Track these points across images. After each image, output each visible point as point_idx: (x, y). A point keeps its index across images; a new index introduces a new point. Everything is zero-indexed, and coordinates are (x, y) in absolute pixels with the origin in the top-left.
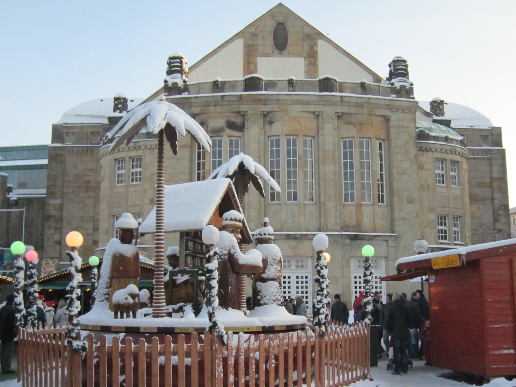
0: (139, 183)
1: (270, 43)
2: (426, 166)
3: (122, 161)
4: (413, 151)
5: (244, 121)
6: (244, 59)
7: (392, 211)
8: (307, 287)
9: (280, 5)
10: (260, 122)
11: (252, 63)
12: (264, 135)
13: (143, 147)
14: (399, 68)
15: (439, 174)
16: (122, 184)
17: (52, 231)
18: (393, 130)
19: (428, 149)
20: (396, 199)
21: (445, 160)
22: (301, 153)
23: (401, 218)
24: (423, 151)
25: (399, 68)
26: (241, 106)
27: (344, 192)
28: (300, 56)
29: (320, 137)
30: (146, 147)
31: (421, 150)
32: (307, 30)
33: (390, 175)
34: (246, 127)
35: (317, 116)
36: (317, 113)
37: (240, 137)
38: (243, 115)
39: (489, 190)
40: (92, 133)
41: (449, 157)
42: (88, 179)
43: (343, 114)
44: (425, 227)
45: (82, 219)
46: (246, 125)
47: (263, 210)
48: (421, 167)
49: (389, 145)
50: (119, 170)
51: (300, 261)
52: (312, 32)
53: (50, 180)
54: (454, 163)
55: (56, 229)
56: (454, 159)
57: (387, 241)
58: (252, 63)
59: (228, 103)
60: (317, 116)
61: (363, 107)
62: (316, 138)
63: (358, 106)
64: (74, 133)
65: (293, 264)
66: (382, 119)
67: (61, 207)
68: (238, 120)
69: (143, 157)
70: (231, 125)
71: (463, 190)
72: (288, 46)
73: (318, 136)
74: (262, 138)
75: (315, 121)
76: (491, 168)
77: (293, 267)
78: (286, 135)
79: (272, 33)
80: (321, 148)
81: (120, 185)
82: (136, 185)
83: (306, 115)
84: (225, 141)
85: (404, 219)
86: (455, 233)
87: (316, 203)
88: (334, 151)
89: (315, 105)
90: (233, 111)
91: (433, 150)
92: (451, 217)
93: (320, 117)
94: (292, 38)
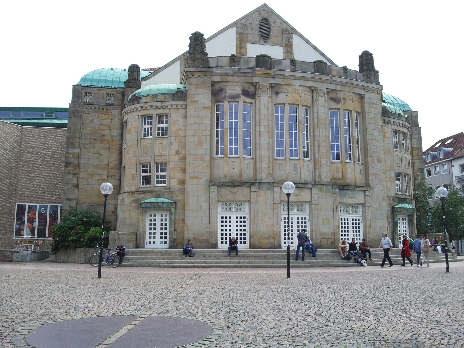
0: (164, 136)
1: (257, 33)
2: (387, 135)
3: (148, 117)
4: (381, 123)
5: (256, 90)
6: (237, 44)
8: (222, 226)
9: (265, 5)
10: (269, 93)
13: (169, 107)
14: (366, 60)
17: (71, 176)
18: (366, 105)
19: (389, 122)
20: (370, 159)
21: (399, 131)
24: (385, 123)
25: (366, 60)
26: (254, 78)
28: (280, 45)
29: (315, 108)
30: (172, 106)
32: (285, 26)
34: (257, 96)
35: (312, 90)
37: (252, 103)
38: (255, 86)
40: (107, 94)
41: (402, 129)
42: (104, 132)
43: (332, 90)
45: (97, 166)
46: (257, 93)
47: (271, 164)
48: (385, 136)
51: (239, 205)
53: (70, 132)
55: (74, 174)
57: (365, 191)
59: (243, 75)
62: (311, 108)
63: (342, 85)
64: (91, 93)
65: (234, 207)
67: (79, 156)
68: (252, 89)
69: (169, 115)
70: (246, 93)
72: (270, 37)
74: (270, 104)
75: (310, 94)
77: (234, 210)
78: (289, 104)
79: (259, 25)
80: (315, 116)
82: (163, 138)
85: (375, 175)
89: (311, 81)
90: (247, 81)
92: (403, 174)
93: (315, 91)
94: (274, 30)
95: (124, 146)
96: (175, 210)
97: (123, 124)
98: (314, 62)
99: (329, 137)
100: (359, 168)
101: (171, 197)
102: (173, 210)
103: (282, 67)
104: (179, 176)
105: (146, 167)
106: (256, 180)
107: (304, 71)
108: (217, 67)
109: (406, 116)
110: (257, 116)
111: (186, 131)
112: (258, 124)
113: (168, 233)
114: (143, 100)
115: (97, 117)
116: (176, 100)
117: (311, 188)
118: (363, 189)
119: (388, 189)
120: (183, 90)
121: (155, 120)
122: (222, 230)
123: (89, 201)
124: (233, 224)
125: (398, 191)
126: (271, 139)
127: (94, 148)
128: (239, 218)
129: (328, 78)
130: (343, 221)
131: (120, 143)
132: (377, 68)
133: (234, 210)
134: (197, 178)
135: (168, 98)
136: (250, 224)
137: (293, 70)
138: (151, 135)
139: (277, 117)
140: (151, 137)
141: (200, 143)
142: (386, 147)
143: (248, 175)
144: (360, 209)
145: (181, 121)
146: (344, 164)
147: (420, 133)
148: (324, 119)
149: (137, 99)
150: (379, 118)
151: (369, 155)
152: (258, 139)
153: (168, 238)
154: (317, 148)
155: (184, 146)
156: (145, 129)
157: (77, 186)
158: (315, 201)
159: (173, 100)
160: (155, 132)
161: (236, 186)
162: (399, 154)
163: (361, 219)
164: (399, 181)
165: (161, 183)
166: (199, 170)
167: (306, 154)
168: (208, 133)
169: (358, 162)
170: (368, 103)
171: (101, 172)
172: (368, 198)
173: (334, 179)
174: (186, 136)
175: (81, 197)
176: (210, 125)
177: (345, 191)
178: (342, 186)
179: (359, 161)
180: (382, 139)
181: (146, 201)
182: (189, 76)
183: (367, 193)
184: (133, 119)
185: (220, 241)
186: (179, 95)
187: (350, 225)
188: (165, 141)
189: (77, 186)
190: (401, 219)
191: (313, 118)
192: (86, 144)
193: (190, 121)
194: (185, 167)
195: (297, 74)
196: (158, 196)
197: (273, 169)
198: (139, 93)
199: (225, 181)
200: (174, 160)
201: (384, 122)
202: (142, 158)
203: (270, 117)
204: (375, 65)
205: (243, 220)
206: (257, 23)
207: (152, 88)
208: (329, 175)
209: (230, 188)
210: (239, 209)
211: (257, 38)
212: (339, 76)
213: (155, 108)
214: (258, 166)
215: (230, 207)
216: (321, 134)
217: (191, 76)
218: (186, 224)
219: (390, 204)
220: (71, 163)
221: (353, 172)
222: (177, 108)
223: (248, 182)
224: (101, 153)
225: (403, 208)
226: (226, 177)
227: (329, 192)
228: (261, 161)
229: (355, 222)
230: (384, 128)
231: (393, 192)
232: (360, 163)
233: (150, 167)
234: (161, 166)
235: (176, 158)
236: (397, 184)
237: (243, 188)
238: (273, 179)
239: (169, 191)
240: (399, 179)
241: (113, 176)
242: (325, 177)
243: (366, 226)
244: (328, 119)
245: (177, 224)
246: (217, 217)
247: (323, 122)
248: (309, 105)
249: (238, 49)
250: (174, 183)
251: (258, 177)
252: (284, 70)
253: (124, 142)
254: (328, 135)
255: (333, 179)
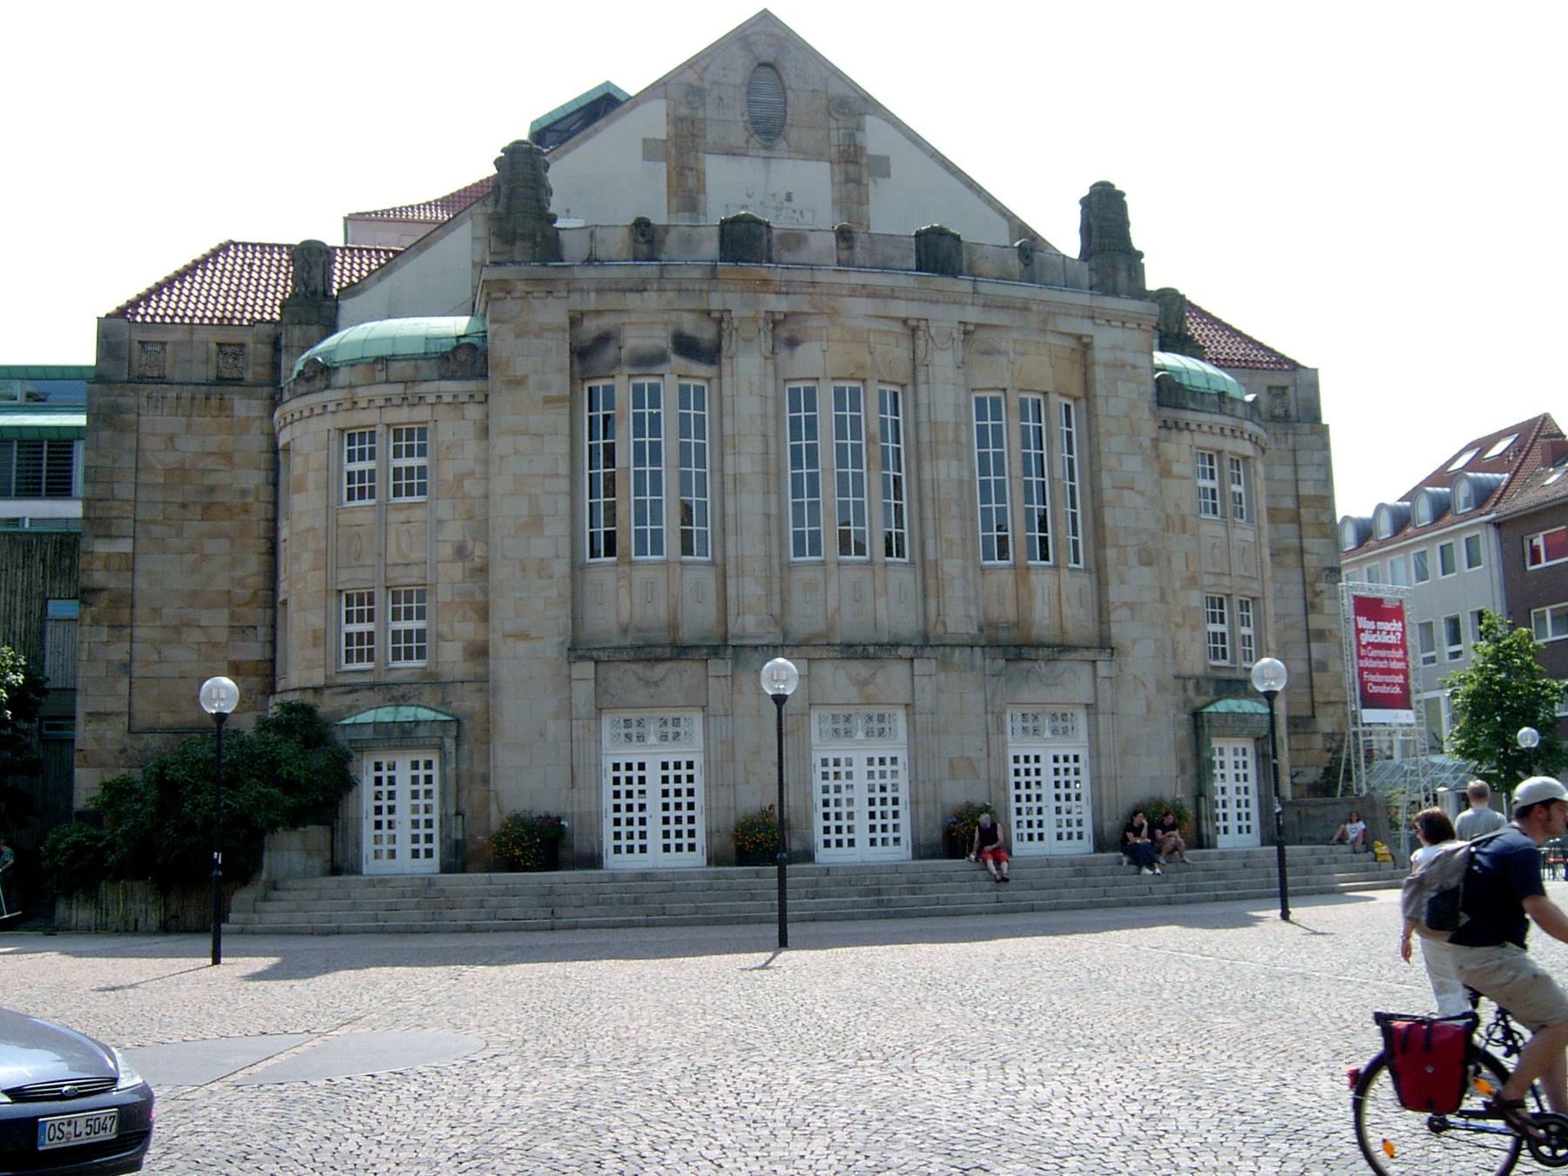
0: (416, 499)
2: (1177, 469)
4: (1148, 428)
5: (720, 337)
7: (1101, 584)
8: (617, 795)
9: (765, 16)
10: (765, 342)
11: (691, 169)
12: (776, 378)
13: (431, 399)
14: (1104, 212)
15: (1205, 489)
16: (362, 503)
18: (1100, 374)
19: (1182, 425)
20: (1111, 553)
21: (1219, 452)
22: (875, 427)
23: (1125, 604)
25: (1104, 212)
27: (791, 530)
28: (819, 157)
29: (922, 388)
30: (439, 397)
31: (1165, 425)
33: (1095, 490)
34: (724, 353)
35: (912, 329)
36: (913, 323)
37: (709, 380)
38: (720, 320)
39: (1291, 528)
41: (1229, 445)
42: (210, 480)
44: (1178, 626)
45: (193, 597)
47: (776, 581)
48: (1166, 472)
49: (1091, 414)
50: (351, 459)
52: (852, 94)
54: (1239, 461)
55: (112, 627)
56: (1239, 451)
58: (691, 169)
60: (912, 329)
61: (1026, 309)
62: (910, 387)
64: (164, 344)
66: (1072, 343)
67: (129, 563)
68: (706, 333)
69: (431, 426)
70: (686, 346)
71: (1259, 535)
73: (915, 383)
74: (770, 382)
75: (905, 342)
76: (1296, 472)
79: (744, 90)
81: (356, 503)
83: (882, 325)
84: (669, 389)
85: (1131, 606)
86: (1246, 640)
87: (912, 563)
88: (957, 424)
91: (1193, 427)
93: (920, 333)
95: (284, 532)
96: (457, 745)
97: (275, 455)
98: (918, 235)
99: (971, 483)
100: (1076, 583)
101: (443, 702)
102: (449, 744)
103: (804, 256)
104: (468, 630)
105: (360, 604)
106: (726, 639)
107: (884, 267)
108: (590, 260)
109: (1249, 398)
110: (727, 422)
111: (487, 478)
112: (729, 450)
113: (436, 824)
114: (343, 377)
115: (189, 426)
116: (452, 378)
117: (912, 659)
118: (1090, 655)
119: (1181, 650)
120: (475, 341)
121: (384, 443)
122: (617, 808)
123: (167, 719)
124: (654, 786)
125: (1216, 658)
126: (773, 499)
127: (179, 534)
128: (671, 766)
129: (963, 285)
130: (1022, 766)
131: (270, 516)
132: (1137, 244)
133: (652, 739)
134: (525, 636)
135: (427, 369)
136: (708, 786)
137: (844, 264)
138: (372, 496)
139: (795, 423)
140: (372, 502)
141: (535, 523)
142: (1171, 510)
143: (699, 619)
144: (1081, 722)
145: (472, 448)
146: (1022, 573)
147: (1326, 446)
148: (951, 427)
149: (322, 373)
150: (1146, 415)
151: (1109, 541)
152: (729, 499)
153: (436, 838)
154: (929, 523)
155: (482, 528)
156: (350, 475)
157: (127, 667)
158: (925, 701)
159: (442, 378)
160: (384, 485)
161: (659, 660)
162: (1221, 531)
163: (1084, 755)
164: (1222, 622)
165: (409, 657)
166: (531, 610)
167: (893, 546)
168: (564, 485)
169: (1072, 565)
170: (1106, 365)
171: (206, 617)
172: (1104, 686)
173: (990, 625)
174: (486, 497)
175: (140, 704)
176: (567, 458)
177: (1026, 665)
178: (1014, 648)
179: (1077, 561)
180: (1153, 487)
181: (361, 719)
182: (493, 295)
183: (1102, 669)
184: (309, 434)
185: (609, 843)
186: (464, 360)
187: (1048, 778)
188: (417, 514)
189: (127, 667)
190: (1228, 752)
191: (917, 424)
192: (153, 522)
193: (502, 445)
194: (487, 603)
195: (856, 279)
196: (399, 701)
197: (783, 601)
198: (329, 353)
199: (623, 643)
200: (449, 579)
201: (1165, 425)
202: (344, 575)
203: (771, 423)
204: (1131, 230)
205: (684, 772)
206: (739, 81)
207: (373, 335)
208: (973, 611)
209: (638, 668)
210: (670, 736)
211: (737, 136)
212: (1004, 277)
213: (382, 403)
214: (731, 591)
215: (640, 730)
216: (942, 476)
217: (501, 295)
218: (497, 793)
219: (1185, 703)
220: (102, 590)
221: (1053, 598)
222: (457, 404)
223: (698, 647)
224: (207, 551)
225: (1233, 713)
226: (624, 630)
227: (972, 668)
228: (740, 574)
229: (1061, 765)
230: (1161, 445)
231: (1196, 660)
232: (1081, 566)
233: (371, 602)
234: (410, 600)
235: (457, 570)
236: (1215, 634)
237: (681, 665)
238: (785, 634)
239: (432, 680)
240: (1222, 615)
241: (248, 631)
242: (959, 619)
243: (1099, 778)
244: (969, 424)
245: (465, 793)
246: (598, 764)
247: (951, 437)
248: (900, 379)
249: (674, 174)
250: (451, 658)
251: (734, 627)
252: (812, 267)
253: (281, 513)
254: (966, 478)
255: (988, 625)
